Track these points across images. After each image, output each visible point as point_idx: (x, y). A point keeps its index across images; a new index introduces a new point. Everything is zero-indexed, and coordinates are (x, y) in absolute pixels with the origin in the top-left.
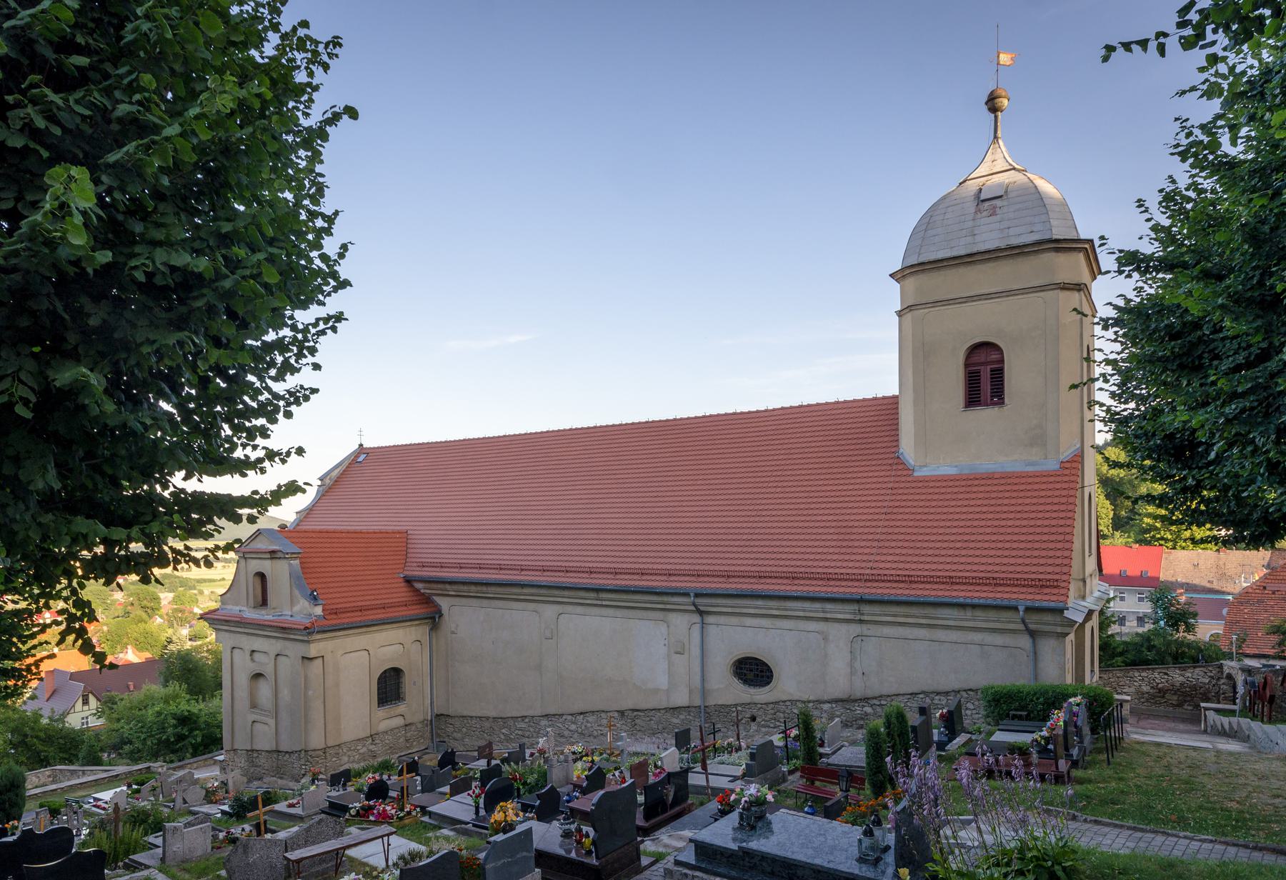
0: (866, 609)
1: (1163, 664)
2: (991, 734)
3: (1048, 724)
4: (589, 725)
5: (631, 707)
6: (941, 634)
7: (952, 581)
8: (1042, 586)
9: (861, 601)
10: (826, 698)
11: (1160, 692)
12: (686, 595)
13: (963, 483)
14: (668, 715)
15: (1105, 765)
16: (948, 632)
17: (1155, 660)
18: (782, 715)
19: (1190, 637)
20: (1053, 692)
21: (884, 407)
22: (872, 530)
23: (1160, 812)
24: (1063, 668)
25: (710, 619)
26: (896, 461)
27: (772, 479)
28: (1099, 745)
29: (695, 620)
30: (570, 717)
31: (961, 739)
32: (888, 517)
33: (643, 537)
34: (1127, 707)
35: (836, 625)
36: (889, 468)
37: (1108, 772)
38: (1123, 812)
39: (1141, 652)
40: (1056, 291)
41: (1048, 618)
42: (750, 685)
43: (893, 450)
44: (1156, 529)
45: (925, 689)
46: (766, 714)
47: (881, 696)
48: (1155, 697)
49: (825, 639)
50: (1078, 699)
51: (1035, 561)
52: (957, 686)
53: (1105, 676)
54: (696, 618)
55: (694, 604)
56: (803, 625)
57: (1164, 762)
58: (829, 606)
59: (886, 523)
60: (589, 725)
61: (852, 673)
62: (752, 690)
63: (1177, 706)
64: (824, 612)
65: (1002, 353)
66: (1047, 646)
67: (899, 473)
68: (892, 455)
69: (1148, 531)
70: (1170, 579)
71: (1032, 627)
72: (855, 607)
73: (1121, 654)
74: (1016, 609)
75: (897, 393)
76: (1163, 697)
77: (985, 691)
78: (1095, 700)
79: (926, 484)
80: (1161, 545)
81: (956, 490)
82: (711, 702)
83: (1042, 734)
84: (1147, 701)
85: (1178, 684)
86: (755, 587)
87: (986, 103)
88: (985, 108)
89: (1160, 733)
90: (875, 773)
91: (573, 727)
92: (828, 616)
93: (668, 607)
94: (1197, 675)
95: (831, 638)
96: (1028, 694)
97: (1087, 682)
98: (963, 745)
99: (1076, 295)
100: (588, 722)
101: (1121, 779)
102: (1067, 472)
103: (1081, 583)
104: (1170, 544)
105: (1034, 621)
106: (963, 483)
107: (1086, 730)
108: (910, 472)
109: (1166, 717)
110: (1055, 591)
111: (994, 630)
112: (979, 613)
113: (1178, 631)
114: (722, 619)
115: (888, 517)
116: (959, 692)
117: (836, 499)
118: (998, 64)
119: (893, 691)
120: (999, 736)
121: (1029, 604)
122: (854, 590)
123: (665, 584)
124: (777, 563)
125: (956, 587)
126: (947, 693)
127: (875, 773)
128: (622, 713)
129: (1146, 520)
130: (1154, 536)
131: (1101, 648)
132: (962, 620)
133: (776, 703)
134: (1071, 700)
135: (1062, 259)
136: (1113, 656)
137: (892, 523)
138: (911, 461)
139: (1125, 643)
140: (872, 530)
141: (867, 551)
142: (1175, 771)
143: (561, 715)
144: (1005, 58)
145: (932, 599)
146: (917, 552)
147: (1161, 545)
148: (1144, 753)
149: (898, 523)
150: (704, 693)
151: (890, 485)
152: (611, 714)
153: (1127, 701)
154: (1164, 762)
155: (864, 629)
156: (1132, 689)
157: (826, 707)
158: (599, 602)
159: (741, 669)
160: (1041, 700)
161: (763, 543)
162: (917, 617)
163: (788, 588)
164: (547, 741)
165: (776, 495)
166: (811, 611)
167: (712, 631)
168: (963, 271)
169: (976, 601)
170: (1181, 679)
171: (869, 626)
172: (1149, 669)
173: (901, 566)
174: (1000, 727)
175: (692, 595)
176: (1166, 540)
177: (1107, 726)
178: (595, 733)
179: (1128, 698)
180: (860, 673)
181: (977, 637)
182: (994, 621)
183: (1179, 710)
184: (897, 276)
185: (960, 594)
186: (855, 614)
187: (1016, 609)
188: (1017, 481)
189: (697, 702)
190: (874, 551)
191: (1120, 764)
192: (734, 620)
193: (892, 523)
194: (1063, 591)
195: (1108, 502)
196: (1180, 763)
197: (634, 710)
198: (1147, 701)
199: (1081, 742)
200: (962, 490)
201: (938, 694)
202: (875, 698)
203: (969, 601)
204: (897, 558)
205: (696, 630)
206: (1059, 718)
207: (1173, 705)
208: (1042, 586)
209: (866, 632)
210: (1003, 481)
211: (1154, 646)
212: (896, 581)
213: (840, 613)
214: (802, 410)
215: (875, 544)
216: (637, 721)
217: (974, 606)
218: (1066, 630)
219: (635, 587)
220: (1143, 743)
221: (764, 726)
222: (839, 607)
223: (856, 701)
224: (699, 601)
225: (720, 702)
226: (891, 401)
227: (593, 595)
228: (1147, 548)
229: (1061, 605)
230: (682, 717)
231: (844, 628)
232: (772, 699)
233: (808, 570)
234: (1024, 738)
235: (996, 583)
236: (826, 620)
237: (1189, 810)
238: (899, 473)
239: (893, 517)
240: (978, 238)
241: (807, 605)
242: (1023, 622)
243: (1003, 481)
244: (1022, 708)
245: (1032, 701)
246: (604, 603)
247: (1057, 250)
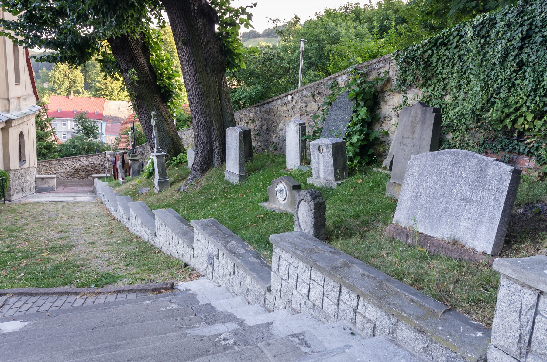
11: (76, 171)
19: (94, 141)
44: (102, 89)
63: (85, 177)
69: (98, 90)
70: (108, 115)
76: (78, 173)
80: (104, 98)
84: (70, 176)
85: (85, 166)
94: (119, 164)
103: (6, 102)
104: (108, 97)
109: (79, 184)
113: (89, 137)
129: (98, 84)
130: (101, 93)
147: (104, 98)
156: (62, 171)
170: (87, 163)
172: (70, 158)
176: (107, 95)
195: (81, 74)
198: (70, 176)
211: (76, 146)
228: (97, 99)
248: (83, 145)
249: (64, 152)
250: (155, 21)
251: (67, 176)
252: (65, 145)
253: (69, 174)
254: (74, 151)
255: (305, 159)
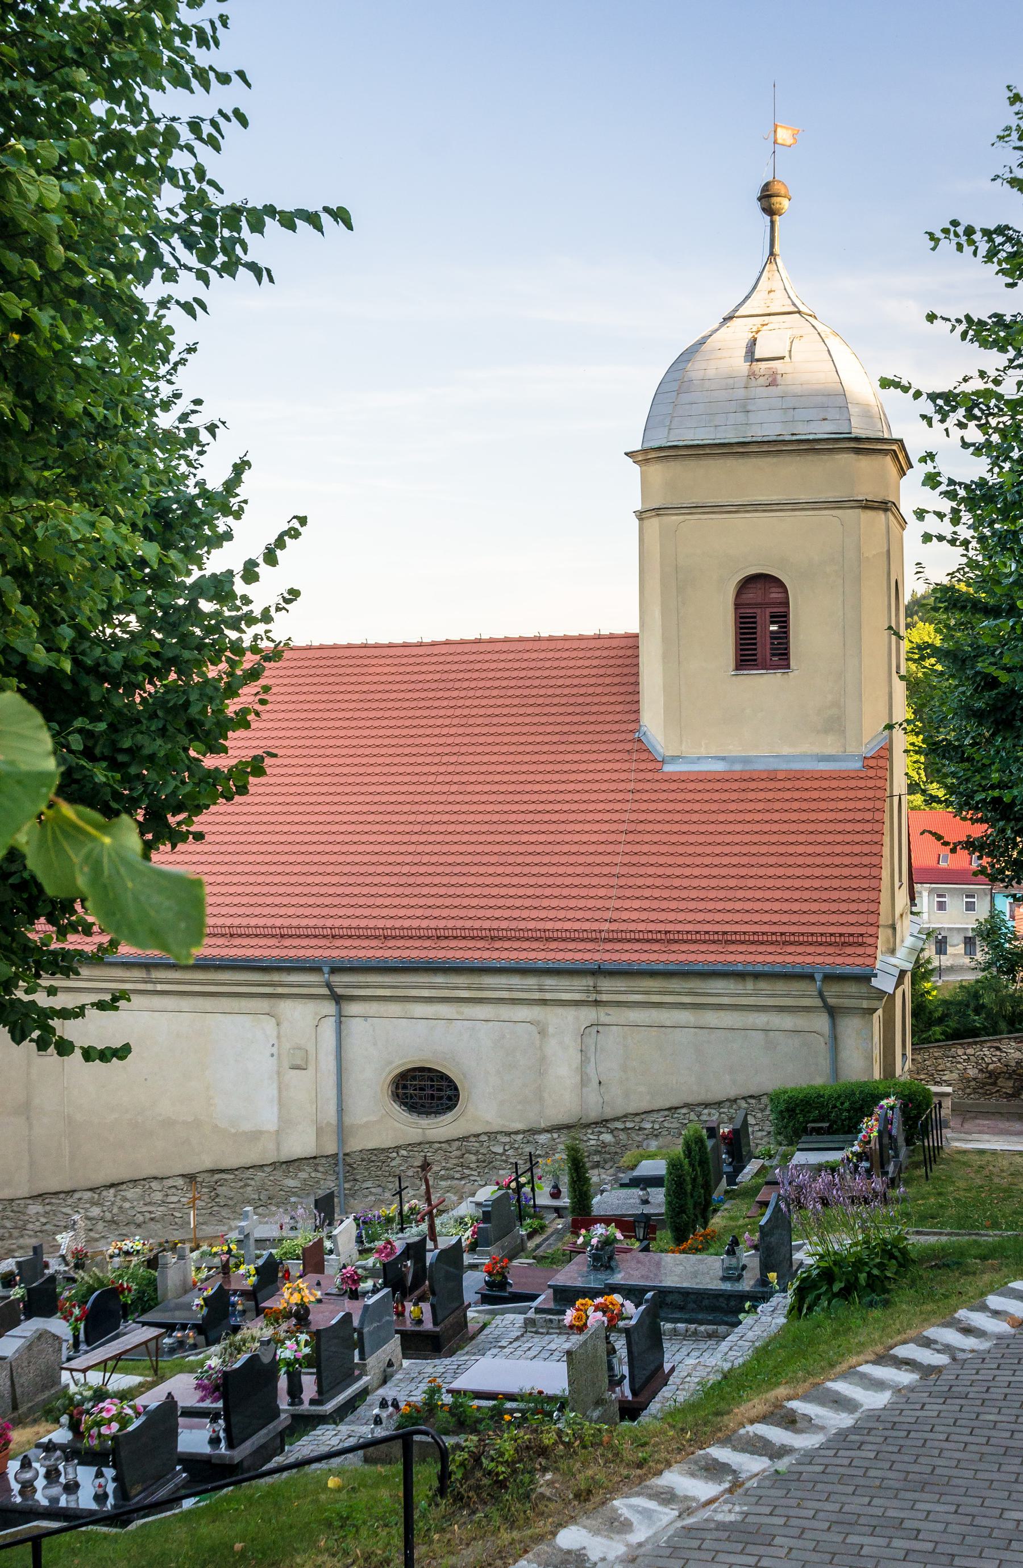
0: (605, 983)
1: (995, 1033)
2: (787, 1157)
3: (860, 1136)
4: (127, 1205)
5: (209, 1165)
6: (711, 1018)
7: (726, 939)
8: (844, 944)
9: (598, 972)
10: (543, 1125)
11: (990, 1077)
12: (316, 969)
13: (735, 786)
14: (278, 1174)
15: (923, 1181)
16: (722, 1013)
17: (985, 1028)
18: (473, 1158)
20: (861, 1092)
21: (613, 653)
22: (607, 859)
23: (977, 1220)
24: (870, 1058)
25: (353, 1008)
26: (636, 746)
27: (442, 769)
28: (916, 1159)
29: (325, 1012)
30: (89, 1194)
31: (752, 1167)
32: (630, 838)
33: (223, 869)
34: (947, 1103)
35: (560, 1010)
36: (626, 756)
37: (927, 1188)
38: (943, 1225)
39: (965, 1015)
40: (857, 510)
41: (852, 988)
42: (419, 1113)
43: (631, 727)
45: (690, 1100)
46: (447, 1159)
47: (625, 1116)
48: (985, 1084)
49: (542, 1032)
50: (891, 1101)
51: (834, 907)
52: (732, 1093)
53: (919, 1058)
54: (329, 1008)
55: (329, 986)
56: (506, 1012)
57: (986, 1172)
58: (549, 982)
59: (628, 848)
60: (127, 1205)
61: (584, 1082)
62: (425, 1122)
63: (1013, 1095)
64: (541, 990)
65: (786, 591)
66: (850, 1027)
67: (642, 766)
68: (630, 737)
71: (831, 1001)
72: (589, 981)
73: (940, 1021)
74: (811, 977)
75: (634, 628)
76: (995, 1084)
77: (774, 1098)
78: (911, 1100)
79: (682, 786)
81: (725, 796)
82: (356, 1144)
83: (854, 1149)
85: (1013, 1064)
86: (432, 954)
87: (760, 199)
88: (757, 206)
89: (986, 1137)
90: (679, 1213)
91: (95, 1211)
92: (548, 996)
93: (280, 990)
95: (551, 1030)
96: (830, 1097)
97: (898, 1072)
98: (757, 1174)
99: (880, 516)
100: (125, 1199)
101: (940, 1194)
102: (871, 773)
103: (890, 931)
105: (834, 994)
106: (735, 786)
107: (901, 1141)
108: (658, 766)
110: (860, 950)
111: (781, 1009)
112: (762, 985)
114: (373, 1008)
115: (630, 838)
116: (735, 1100)
117: (549, 807)
118: (775, 142)
119: (645, 1106)
120: (800, 1158)
121: (828, 970)
122: (587, 956)
123: (275, 953)
124: (463, 913)
125: (732, 948)
126: (719, 1104)
127: (679, 1213)
128: (191, 1178)
131: (914, 1015)
132: (739, 995)
133: (465, 1139)
134: (883, 1102)
135: (864, 464)
136: (930, 1023)
137: (637, 848)
138: (659, 748)
139: (945, 1002)
140: (607, 859)
141: (602, 892)
142: (996, 1180)
143: (71, 1192)
144: (784, 135)
145: (699, 967)
146: (675, 894)
148: (964, 1163)
149: (645, 848)
150: (342, 1130)
151: (631, 786)
152: (170, 1182)
153: (948, 1095)
154: (986, 1172)
155: (602, 1015)
156: (955, 1076)
157: (543, 1138)
158: (149, 987)
159: (405, 1087)
160: (847, 1104)
161: (437, 880)
162: (679, 994)
163: (486, 954)
164: (75, 1238)
165: (451, 798)
166: (518, 990)
167: (358, 1030)
168: (731, 463)
169: (759, 968)
171: (610, 1010)
172: (976, 1043)
173: (653, 916)
174: (800, 1146)
175: (326, 970)
177: (925, 1133)
178: (140, 1218)
179: (949, 1089)
180: (595, 1082)
181: (761, 1019)
182: (782, 996)
183: (1015, 1102)
184: (642, 457)
185: (739, 958)
186: (588, 991)
187: (811, 977)
188: (808, 784)
189: (331, 1148)
190: (613, 892)
191: (939, 1179)
192: (394, 1008)
193: (637, 848)
194: (869, 951)
196: (1002, 1171)
197: (213, 1171)
199: (897, 1156)
200: (734, 796)
201: (707, 1105)
202: (617, 1119)
203: (750, 968)
204: (646, 904)
205: (328, 1028)
206: (871, 1127)
207: (1009, 1096)
208: (844, 944)
209: (604, 1019)
210: (788, 785)
211: (983, 1006)
212: (648, 941)
213: (566, 991)
214: (482, 648)
215: (614, 881)
216: (221, 1190)
217: (757, 976)
218: (874, 1004)
219: (222, 959)
220: (965, 1152)
221: (443, 1178)
222: (564, 982)
223: (588, 1126)
224: (337, 979)
225: (370, 1146)
226: (623, 643)
227: (138, 974)
229: (868, 970)
230: (303, 1175)
231: (570, 1013)
232: (456, 1135)
233: (513, 925)
234: (834, 1157)
235: (785, 940)
236: (544, 1002)
237: (1003, 1216)
238: (642, 766)
239: (638, 838)
240: (753, 418)
241: (515, 980)
242: (821, 995)
243: (788, 785)
244: (821, 1119)
245: (834, 1107)
246: (159, 987)
247: (858, 451)
248: (1001, 1003)
249: (952, 1024)
250: (209, 1362)
251: (968, 1091)
252: (951, 1003)
253: (973, 1083)
254: (978, 1021)
255: (996, 1314)
